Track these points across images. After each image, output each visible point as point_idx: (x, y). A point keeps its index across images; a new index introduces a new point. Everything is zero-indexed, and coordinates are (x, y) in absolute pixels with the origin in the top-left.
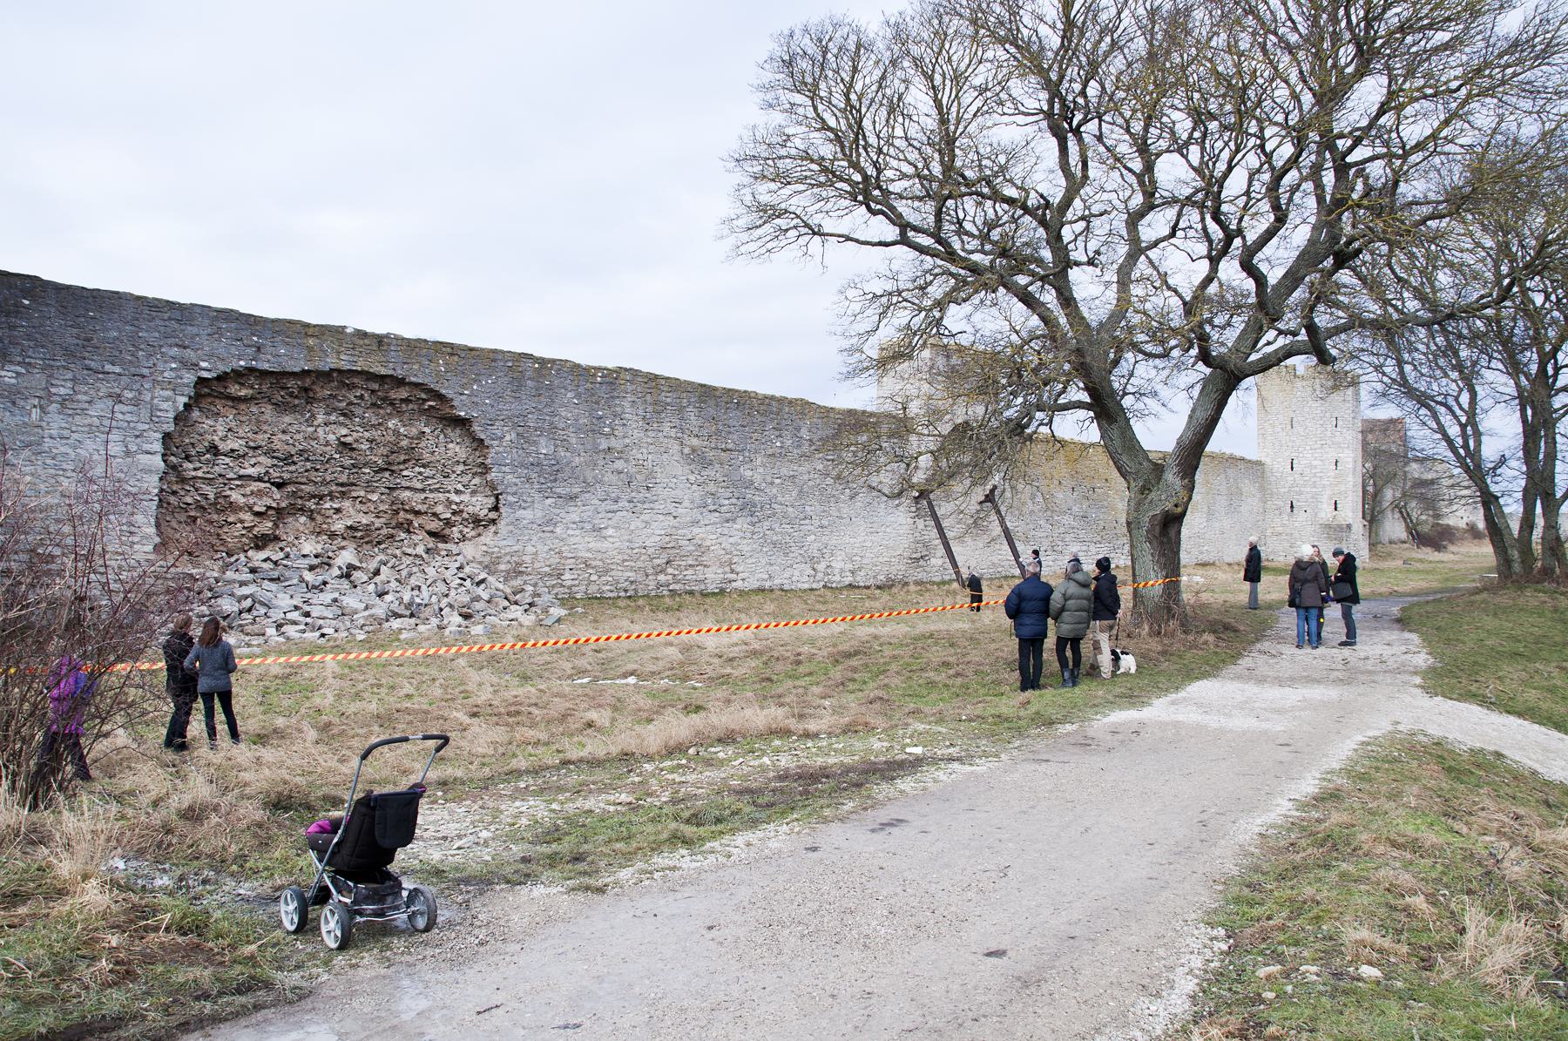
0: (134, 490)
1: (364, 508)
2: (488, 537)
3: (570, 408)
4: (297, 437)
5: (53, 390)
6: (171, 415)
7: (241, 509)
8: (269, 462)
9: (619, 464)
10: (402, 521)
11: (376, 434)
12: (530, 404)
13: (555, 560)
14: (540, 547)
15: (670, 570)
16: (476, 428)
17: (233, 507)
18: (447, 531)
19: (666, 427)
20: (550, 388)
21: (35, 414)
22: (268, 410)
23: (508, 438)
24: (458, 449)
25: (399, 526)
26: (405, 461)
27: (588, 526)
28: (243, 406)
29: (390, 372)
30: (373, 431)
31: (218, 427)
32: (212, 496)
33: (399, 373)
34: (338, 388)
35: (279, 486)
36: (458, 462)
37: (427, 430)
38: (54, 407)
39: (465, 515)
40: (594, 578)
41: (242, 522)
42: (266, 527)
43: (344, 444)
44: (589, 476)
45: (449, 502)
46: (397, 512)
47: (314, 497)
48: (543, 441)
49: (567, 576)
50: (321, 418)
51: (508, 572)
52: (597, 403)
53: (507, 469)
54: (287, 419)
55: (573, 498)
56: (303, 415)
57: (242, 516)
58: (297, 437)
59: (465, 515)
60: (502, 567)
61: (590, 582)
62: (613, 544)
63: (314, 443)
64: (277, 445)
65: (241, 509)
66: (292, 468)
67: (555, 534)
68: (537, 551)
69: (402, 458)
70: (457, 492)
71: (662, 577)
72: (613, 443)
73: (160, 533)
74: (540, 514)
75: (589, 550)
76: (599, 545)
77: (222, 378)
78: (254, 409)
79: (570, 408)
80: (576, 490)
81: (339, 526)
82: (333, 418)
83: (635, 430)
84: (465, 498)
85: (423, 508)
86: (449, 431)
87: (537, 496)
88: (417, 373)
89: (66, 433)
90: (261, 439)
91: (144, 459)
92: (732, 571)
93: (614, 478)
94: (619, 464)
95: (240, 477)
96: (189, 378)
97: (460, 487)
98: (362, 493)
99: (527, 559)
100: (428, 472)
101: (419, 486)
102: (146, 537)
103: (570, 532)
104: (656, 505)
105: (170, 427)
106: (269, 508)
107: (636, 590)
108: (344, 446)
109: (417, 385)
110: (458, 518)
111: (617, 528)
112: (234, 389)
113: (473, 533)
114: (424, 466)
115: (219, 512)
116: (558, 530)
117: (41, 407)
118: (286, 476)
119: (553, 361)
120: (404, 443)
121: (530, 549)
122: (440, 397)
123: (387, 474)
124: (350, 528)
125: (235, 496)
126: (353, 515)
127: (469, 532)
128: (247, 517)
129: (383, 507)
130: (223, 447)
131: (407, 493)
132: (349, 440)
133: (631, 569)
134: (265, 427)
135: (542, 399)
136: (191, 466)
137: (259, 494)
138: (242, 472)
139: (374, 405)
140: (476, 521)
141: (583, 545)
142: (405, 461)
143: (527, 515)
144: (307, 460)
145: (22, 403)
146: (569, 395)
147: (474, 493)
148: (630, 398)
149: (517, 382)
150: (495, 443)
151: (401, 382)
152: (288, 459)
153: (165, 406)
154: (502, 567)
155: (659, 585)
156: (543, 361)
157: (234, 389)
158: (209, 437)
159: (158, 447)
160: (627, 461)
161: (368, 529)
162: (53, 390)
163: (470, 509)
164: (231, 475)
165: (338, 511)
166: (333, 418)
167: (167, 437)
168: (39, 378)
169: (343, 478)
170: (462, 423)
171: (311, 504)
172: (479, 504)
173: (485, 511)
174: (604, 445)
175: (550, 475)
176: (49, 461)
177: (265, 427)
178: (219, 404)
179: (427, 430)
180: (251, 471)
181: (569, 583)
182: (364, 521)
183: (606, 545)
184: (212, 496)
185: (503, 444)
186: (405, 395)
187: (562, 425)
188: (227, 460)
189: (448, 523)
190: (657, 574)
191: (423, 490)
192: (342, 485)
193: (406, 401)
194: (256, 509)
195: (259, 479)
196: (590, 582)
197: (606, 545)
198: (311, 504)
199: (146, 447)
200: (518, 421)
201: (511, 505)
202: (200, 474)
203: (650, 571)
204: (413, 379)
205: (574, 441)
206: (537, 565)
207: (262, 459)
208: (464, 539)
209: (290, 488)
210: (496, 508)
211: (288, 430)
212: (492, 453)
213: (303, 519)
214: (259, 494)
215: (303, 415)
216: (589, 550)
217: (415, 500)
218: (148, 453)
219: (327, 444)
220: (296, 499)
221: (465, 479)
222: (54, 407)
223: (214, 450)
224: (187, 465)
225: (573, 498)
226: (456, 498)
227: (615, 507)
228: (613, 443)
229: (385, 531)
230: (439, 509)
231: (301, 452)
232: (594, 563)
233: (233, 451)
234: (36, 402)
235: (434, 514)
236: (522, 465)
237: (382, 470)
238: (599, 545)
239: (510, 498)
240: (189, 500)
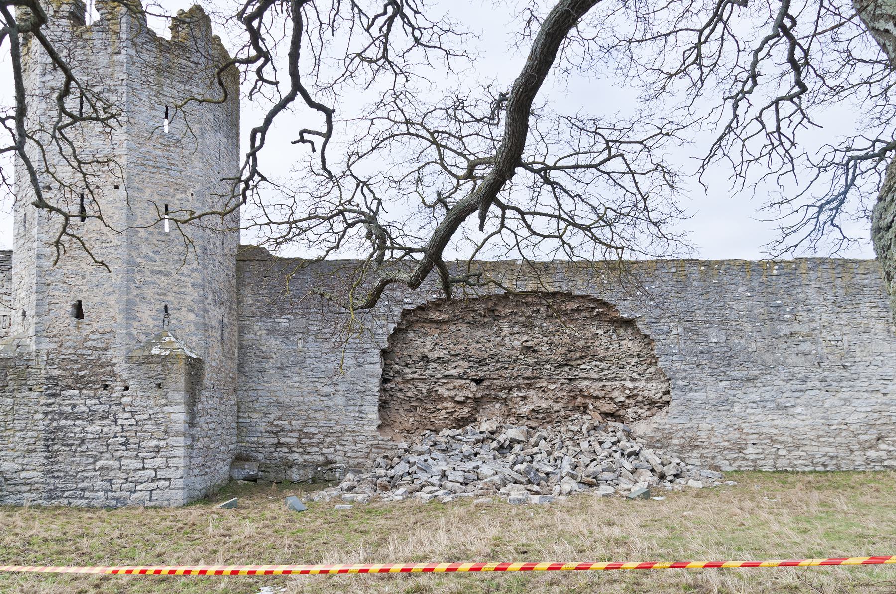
0: (363, 389)
1: (545, 396)
2: (659, 418)
3: (741, 300)
4: (488, 345)
5: (310, 328)
6: (385, 337)
7: (445, 399)
8: (467, 365)
9: (806, 347)
10: (579, 403)
11: (554, 338)
12: (697, 302)
13: (735, 435)
14: (715, 424)
15: (882, 446)
16: (639, 325)
17: (441, 399)
18: (621, 412)
19: (865, 308)
20: (718, 286)
21: (301, 342)
22: (464, 328)
23: (675, 331)
24: (630, 345)
25: (576, 408)
26: (581, 358)
27: (770, 405)
28: (444, 327)
29: (556, 290)
30: (548, 337)
31: (424, 342)
32: (424, 391)
33: (565, 289)
34: (517, 306)
35: (478, 381)
36: (632, 356)
37: (600, 332)
38: (311, 338)
39: (639, 398)
40: (781, 452)
41: (446, 408)
42: (465, 411)
43: (529, 348)
44: (769, 359)
45: (624, 388)
46: (575, 398)
47: (505, 388)
48: (713, 332)
49: (750, 450)
50: (506, 330)
51: (683, 446)
52: (776, 293)
53: (675, 358)
54: (479, 333)
55: (750, 380)
56: (491, 329)
57: (445, 404)
58: (488, 345)
59: (639, 398)
60: (676, 441)
61: (778, 457)
62: (803, 419)
63: (502, 349)
64: (472, 351)
65: (445, 399)
66: (486, 368)
67: (705, 413)
68: (714, 428)
69: (578, 355)
70: (633, 380)
71: (872, 454)
72: (796, 327)
73: (381, 417)
74: (713, 395)
75: (774, 427)
76: (786, 422)
77: (421, 308)
78: (453, 328)
79: (741, 300)
80: (754, 372)
81: (524, 410)
82: (516, 329)
83: (824, 314)
84: (640, 384)
85: (600, 394)
86: (621, 331)
87: (709, 380)
88: (580, 287)
89: (319, 354)
90: (460, 349)
91: (369, 367)
92: (760, 583)
93: (801, 360)
94: (806, 347)
95: (446, 377)
96: (397, 310)
97: (635, 375)
98: (544, 384)
99: (703, 435)
100: (603, 365)
101: (596, 376)
102: (371, 421)
103: (750, 410)
104: (857, 383)
105: (385, 345)
106: (468, 398)
107: (838, 466)
108: (528, 350)
109: (583, 297)
110: (632, 401)
111: (807, 406)
112: (434, 315)
113: (648, 413)
114: (600, 360)
115: (433, 401)
116: (736, 409)
117: (304, 339)
118: (481, 374)
119: (721, 263)
120: (581, 344)
121: (704, 426)
122: (605, 304)
123: (567, 369)
124: (533, 410)
125: (442, 391)
126: (536, 400)
127: (644, 412)
128: (450, 405)
129: (559, 394)
130: (431, 356)
131: (586, 383)
132: (529, 344)
133: (830, 444)
134: (462, 340)
135: (710, 296)
136: (409, 371)
137: (460, 388)
138: (447, 373)
139: (549, 316)
140: (652, 403)
141: (769, 422)
142: (581, 358)
143: (700, 396)
144: (498, 361)
145: (292, 337)
146: (741, 289)
147: (649, 380)
148: (814, 285)
149: (683, 286)
150: (661, 337)
151: (569, 296)
152: (481, 362)
153: (380, 331)
154: (676, 441)
155: (868, 461)
156: (709, 264)
157: (434, 315)
158: (421, 350)
159: (377, 359)
160: (815, 343)
161: (547, 411)
162: (310, 328)
163: (646, 393)
164: (439, 376)
165: (524, 398)
166: (516, 329)
167: (384, 353)
168: (301, 321)
169: (528, 373)
170: (629, 323)
171: (503, 394)
172: (653, 389)
173: (658, 395)
174: (785, 329)
175: (724, 361)
176: (309, 373)
177: (462, 340)
178: (427, 327)
179: (600, 332)
180: (453, 372)
181: (753, 457)
182: (544, 405)
183: (794, 422)
184: (424, 391)
185: (670, 337)
186: (575, 306)
187: (733, 317)
188: (435, 365)
189: (622, 405)
190: (865, 449)
191: (600, 380)
192: (528, 378)
193: (578, 310)
194: (457, 399)
195: (460, 377)
196: (778, 457)
197: (794, 422)
198: (503, 394)
199: (370, 359)
200: (686, 318)
201: (681, 388)
202: (415, 376)
203: (856, 447)
204: (577, 293)
205: (749, 329)
206: (713, 440)
207: (461, 363)
208: (639, 418)
209: (486, 383)
210: (667, 392)
211: (479, 340)
212: (657, 346)
213: (498, 405)
214: (460, 388)
215: (491, 329)
216: (774, 427)
217: (595, 388)
218: (372, 363)
219: (513, 348)
220: (488, 389)
221: (640, 369)
222: (311, 338)
223: (424, 358)
224: (407, 370)
225: (750, 380)
226: (630, 385)
227: (804, 387)
228: (796, 327)
229: (562, 413)
230: (615, 394)
231: (492, 357)
232: (781, 439)
233: (439, 358)
234: (300, 336)
235: (611, 399)
236: (691, 354)
237: (560, 366)
238: (786, 422)
239: (680, 383)
240: (409, 394)
